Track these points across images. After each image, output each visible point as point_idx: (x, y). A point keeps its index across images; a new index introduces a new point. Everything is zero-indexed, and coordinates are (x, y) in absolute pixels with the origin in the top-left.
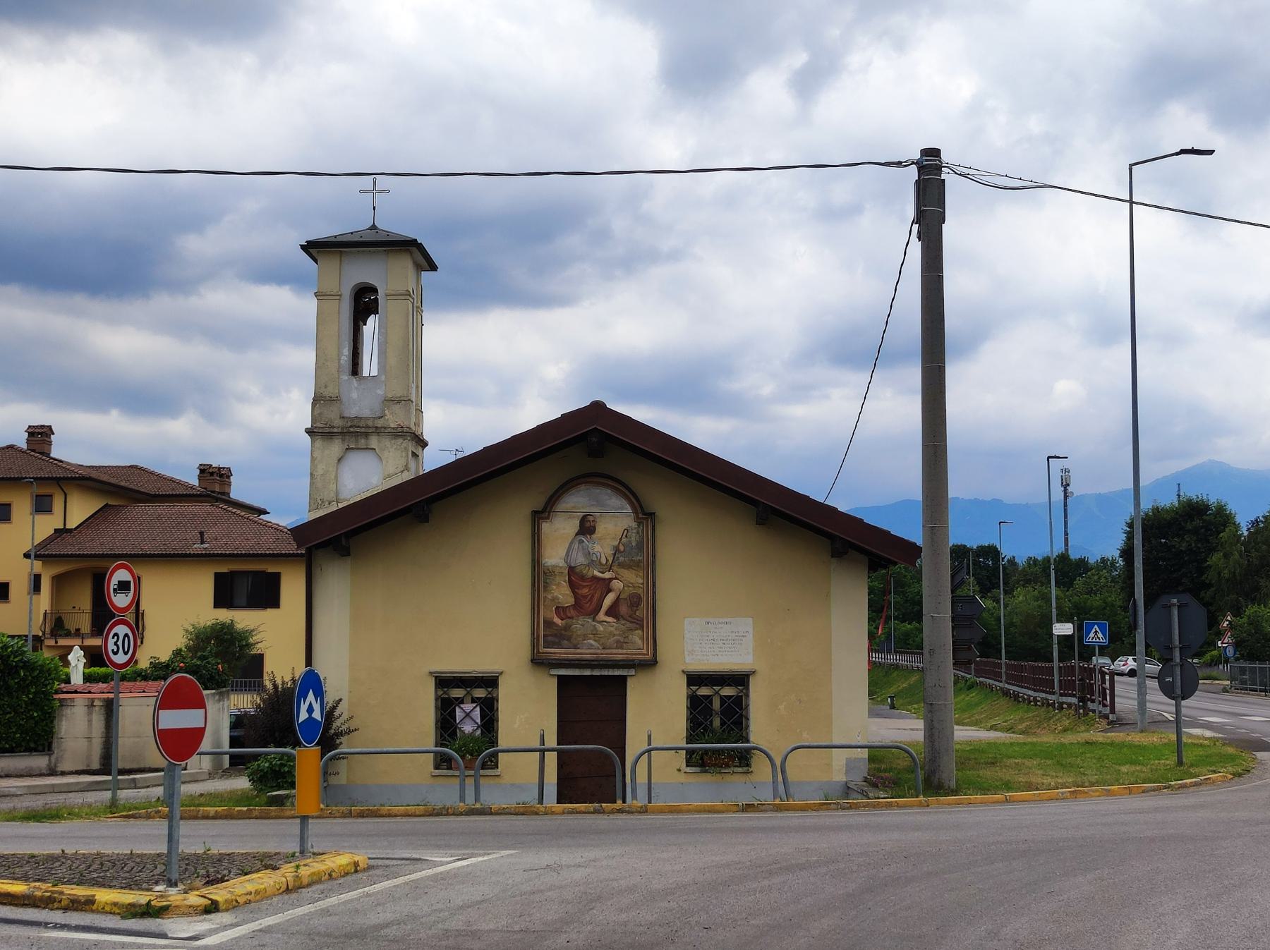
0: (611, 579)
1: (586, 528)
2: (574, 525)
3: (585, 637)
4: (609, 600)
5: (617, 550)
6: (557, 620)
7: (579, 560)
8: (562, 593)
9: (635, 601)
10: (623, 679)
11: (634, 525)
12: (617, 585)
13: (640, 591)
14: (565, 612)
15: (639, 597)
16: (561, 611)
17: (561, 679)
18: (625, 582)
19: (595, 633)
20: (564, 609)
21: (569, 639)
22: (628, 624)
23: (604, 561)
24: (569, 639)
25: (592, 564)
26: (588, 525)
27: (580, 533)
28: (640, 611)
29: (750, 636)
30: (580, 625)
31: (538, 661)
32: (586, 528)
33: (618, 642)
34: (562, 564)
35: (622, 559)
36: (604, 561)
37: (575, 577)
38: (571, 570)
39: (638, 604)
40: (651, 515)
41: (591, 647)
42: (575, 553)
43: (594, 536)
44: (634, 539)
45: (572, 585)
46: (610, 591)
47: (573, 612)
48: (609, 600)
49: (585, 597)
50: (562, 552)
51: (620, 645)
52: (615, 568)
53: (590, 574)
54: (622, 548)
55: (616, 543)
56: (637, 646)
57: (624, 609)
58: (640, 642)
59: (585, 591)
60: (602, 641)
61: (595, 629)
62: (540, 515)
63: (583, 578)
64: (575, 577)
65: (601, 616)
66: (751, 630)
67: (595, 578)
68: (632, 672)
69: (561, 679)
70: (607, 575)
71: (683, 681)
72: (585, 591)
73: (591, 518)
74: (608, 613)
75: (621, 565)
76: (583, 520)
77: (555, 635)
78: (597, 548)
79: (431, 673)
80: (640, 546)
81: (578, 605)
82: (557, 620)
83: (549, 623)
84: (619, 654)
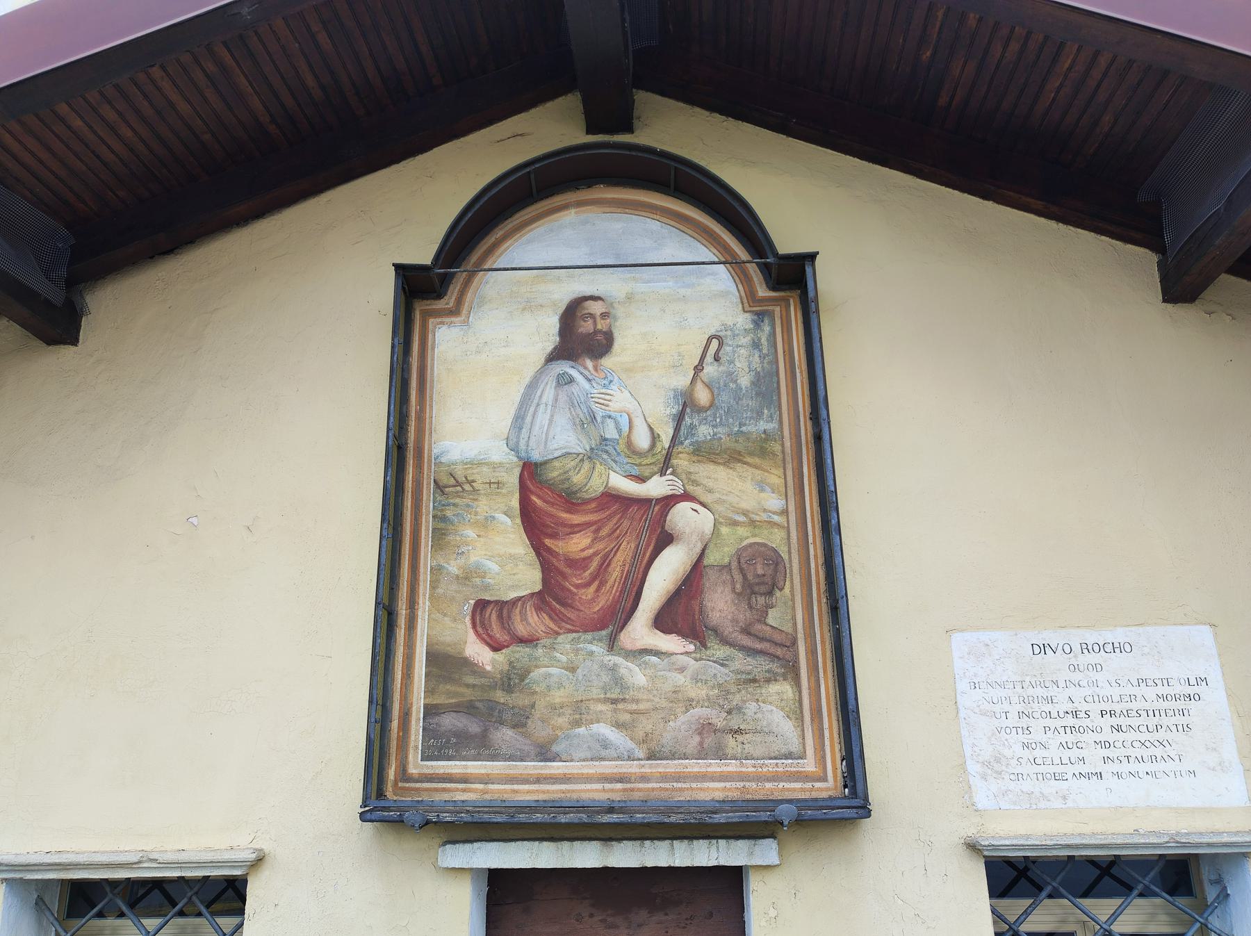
0: (669, 501)
1: (581, 338)
2: (544, 331)
3: (580, 713)
4: (666, 572)
5: (686, 405)
6: (477, 651)
7: (557, 438)
8: (498, 554)
9: (758, 576)
10: (729, 884)
11: (743, 320)
12: (683, 517)
13: (776, 539)
14: (505, 621)
15: (775, 561)
16: (490, 615)
17: (503, 890)
18: (729, 507)
19: (618, 696)
20: (505, 608)
21: (520, 722)
22: (741, 661)
23: (642, 440)
24: (520, 722)
25: (600, 450)
26: (586, 327)
27: (556, 355)
28: (797, 610)
29: (1215, 697)
30: (564, 667)
31: (389, 808)
32: (581, 338)
33: (705, 728)
34: (499, 453)
35: (704, 431)
36: (642, 440)
37: (543, 501)
38: (531, 473)
39: (771, 587)
40: (790, 276)
41: (602, 749)
42: (543, 418)
43: (607, 362)
44: (743, 365)
45: (535, 525)
46: (665, 540)
47: (533, 622)
48: (666, 572)
49: (578, 564)
50: (502, 420)
51: (712, 741)
52: (681, 461)
53: (596, 486)
54: (702, 396)
55: (683, 381)
56: (780, 745)
57: (720, 604)
58: (786, 728)
59: (578, 544)
60: (645, 725)
61: (618, 681)
62: (423, 290)
63: (570, 500)
64: (543, 501)
65: (640, 631)
66: (1215, 676)
67: (611, 499)
68: (766, 852)
69: (503, 890)
70: (657, 487)
71: (974, 884)
72: (578, 544)
73: (596, 308)
74: (664, 621)
75: (704, 452)
76: (572, 313)
77: (469, 708)
78: (620, 400)
79: (973, 847)
80: (765, 387)
81: (552, 596)
82: (477, 651)
83: (445, 664)
84: (711, 782)
